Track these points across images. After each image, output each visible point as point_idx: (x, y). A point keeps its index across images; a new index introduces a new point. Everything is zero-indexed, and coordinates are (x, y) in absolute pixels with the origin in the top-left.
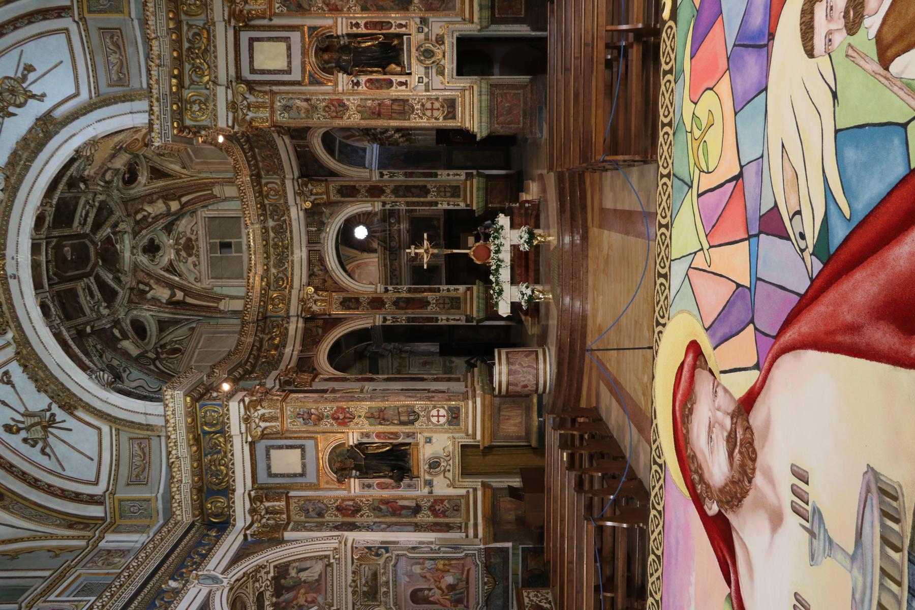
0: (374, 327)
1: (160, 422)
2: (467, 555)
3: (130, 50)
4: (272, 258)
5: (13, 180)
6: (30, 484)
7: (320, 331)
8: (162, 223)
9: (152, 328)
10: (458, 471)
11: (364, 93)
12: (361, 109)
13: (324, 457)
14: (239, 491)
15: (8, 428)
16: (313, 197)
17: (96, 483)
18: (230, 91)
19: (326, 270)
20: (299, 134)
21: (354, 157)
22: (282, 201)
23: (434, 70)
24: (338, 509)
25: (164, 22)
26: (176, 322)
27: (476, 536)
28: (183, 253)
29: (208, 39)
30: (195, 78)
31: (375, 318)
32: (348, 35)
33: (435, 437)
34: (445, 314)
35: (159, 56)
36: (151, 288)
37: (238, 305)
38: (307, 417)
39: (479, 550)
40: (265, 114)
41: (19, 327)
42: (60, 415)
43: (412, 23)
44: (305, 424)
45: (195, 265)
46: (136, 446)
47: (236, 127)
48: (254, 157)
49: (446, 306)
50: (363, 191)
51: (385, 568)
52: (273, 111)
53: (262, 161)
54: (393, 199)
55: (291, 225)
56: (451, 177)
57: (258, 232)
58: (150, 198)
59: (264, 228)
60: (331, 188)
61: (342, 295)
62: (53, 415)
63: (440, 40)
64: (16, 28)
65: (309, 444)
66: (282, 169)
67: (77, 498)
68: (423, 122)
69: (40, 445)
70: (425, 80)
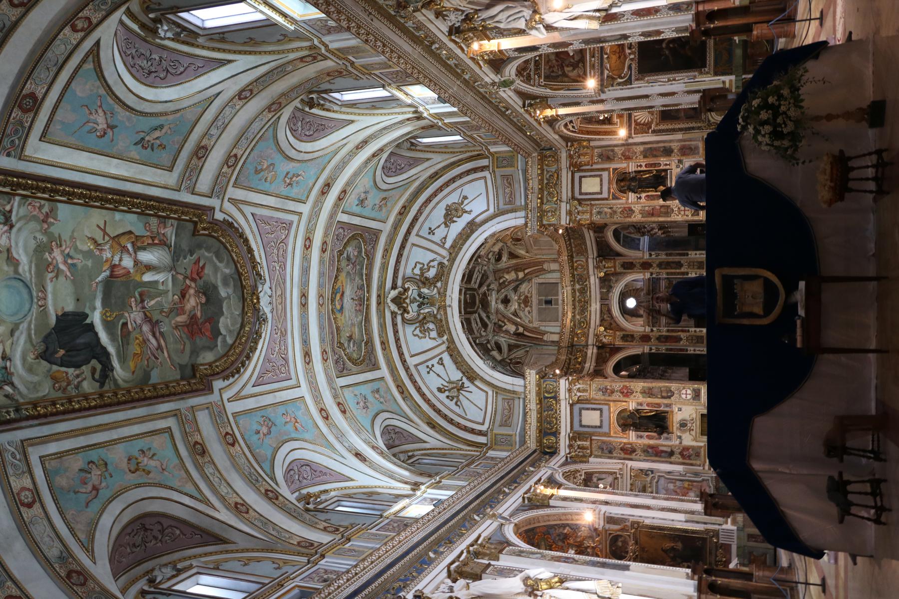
0: (643, 354)
1: (521, 389)
2: (703, 480)
3: (516, 186)
5: (453, 255)
6: (448, 422)
7: (608, 355)
8: (513, 285)
9: (505, 348)
10: (699, 431)
11: (644, 203)
12: (642, 212)
13: (614, 417)
15: (439, 390)
16: (605, 270)
17: (483, 424)
18: (568, 205)
19: (612, 317)
20: (599, 229)
21: (632, 244)
22: (585, 272)
24: (622, 449)
26: (517, 346)
28: (522, 305)
29: (558, 178)
30: (549, 199)
33: (684, 408)
34: (693, 346)
36: (505, 324)
37: (555, 338)
38: (605, 391)
40: (587, 216)
41: (450, 333)
42: (467, 383)
43: (673, 163)
44: (603, 395)
45: (529, 313)
48: (570, 244)
50: (638, 265)
51: (650, 483)
53: (575, 247)
54: (658, 270)
55: (590, 288)
56: (698, 256)
57: (570, 292)
58: (507, 270)
59: (573, 289)
62: (463, 383)
64: (461, 178)
65: (605, 408)
67: (472, 431)
68: (679, 218)
69: (455, 400)
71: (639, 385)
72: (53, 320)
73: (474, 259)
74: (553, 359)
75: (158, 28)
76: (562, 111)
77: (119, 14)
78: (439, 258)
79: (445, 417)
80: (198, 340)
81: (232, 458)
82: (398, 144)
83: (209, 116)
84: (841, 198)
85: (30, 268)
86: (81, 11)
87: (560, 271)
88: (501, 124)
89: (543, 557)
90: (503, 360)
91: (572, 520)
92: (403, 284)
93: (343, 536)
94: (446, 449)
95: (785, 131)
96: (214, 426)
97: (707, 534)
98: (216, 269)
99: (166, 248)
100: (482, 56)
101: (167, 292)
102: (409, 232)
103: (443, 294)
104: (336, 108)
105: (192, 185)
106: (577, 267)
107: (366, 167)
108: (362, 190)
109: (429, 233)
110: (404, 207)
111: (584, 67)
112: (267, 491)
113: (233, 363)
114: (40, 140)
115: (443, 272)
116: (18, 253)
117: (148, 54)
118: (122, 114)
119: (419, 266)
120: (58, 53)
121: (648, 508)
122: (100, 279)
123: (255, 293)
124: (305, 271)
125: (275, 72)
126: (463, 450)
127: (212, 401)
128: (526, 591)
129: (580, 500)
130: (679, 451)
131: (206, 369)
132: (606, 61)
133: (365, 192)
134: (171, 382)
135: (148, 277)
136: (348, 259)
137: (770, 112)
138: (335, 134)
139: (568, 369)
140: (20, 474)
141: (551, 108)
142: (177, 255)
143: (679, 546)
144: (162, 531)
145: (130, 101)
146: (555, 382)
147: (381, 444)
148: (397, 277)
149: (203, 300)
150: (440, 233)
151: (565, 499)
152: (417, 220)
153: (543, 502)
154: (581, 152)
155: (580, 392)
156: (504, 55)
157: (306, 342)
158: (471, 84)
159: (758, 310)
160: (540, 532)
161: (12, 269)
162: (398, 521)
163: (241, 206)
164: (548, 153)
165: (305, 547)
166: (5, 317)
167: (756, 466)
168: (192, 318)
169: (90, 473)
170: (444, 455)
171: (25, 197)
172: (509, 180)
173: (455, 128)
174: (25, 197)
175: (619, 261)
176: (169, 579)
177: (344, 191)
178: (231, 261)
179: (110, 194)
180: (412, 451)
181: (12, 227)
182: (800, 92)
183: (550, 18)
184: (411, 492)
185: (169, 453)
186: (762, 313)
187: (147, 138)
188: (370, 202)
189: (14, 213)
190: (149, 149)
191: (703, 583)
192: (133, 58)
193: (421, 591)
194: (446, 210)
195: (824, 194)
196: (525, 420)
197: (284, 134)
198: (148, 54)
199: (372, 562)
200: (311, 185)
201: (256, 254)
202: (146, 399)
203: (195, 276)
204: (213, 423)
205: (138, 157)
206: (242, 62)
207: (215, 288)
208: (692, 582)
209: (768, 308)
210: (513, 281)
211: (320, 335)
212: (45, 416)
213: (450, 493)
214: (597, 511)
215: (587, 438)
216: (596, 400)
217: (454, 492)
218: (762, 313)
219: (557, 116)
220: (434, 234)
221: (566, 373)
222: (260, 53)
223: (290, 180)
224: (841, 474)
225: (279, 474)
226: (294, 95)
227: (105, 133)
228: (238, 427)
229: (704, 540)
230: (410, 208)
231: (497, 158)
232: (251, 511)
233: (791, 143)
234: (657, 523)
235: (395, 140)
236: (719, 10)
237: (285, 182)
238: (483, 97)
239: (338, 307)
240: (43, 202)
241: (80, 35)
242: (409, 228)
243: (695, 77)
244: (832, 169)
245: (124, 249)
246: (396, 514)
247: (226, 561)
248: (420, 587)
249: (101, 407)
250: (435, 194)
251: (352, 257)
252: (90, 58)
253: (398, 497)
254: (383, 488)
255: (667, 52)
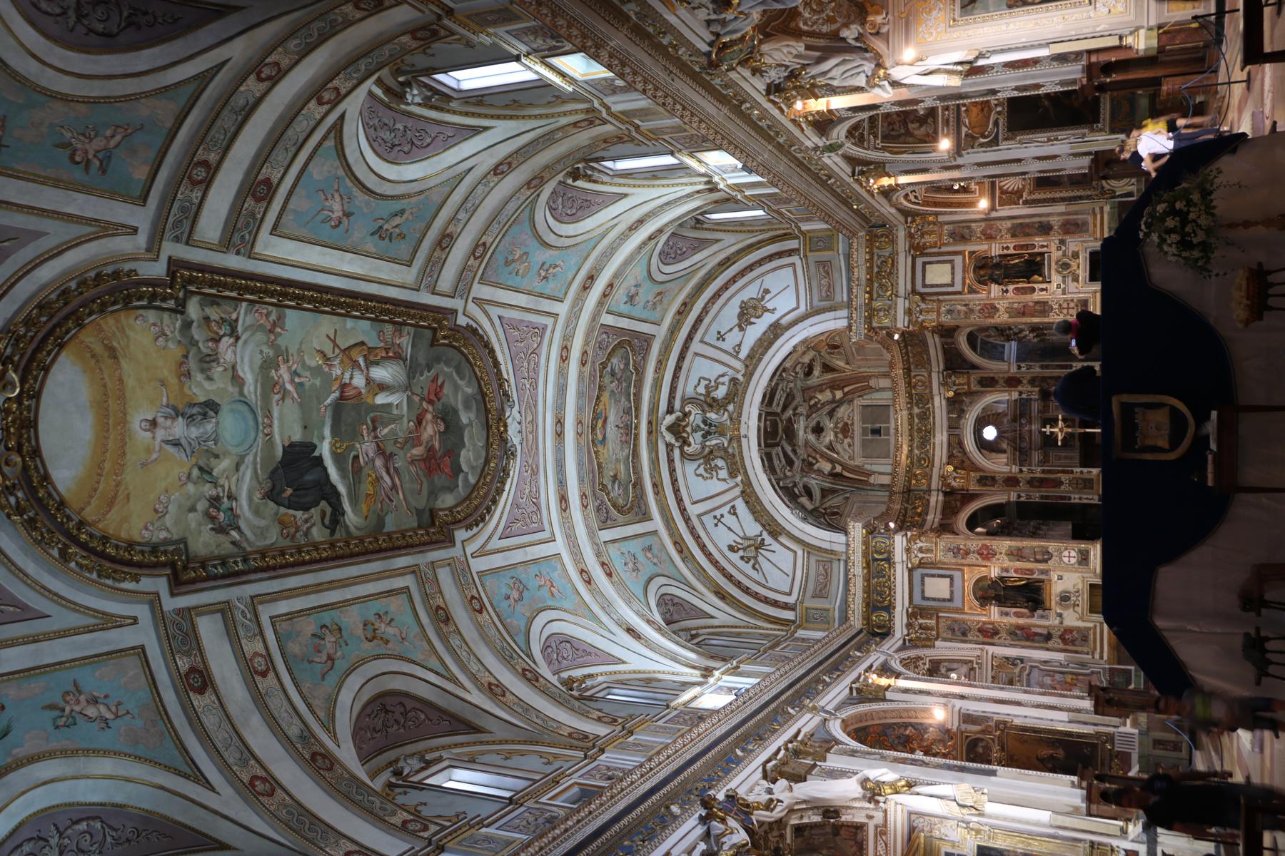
0: (1008, 503)
1: (842, 549)
2: (1093, 673)
3: (836, 275)
4: (916, 440)
5: (751, 368)
6: (743, 591)
7: (958, 504)
8: (827, 409)
9: (817, 494)
10: (1086, 606)
13: (969, 587)
14: (899, 608)
15: (731, 548)
16: (955, 388)
17: (790, 594)
18: (907, 301)
19: (964, 452)
20: (947, 333)
21: (992, 352)
22: (927, 391)
23: (1070, 278)
24: (980, 630)
25: (863, 255)
26: (833, 491)
27: (1101, 657)
28: (840, 436)
31: (1009, 495)
32: (1000, 256)
34: (1079, 493)
35: (858, 279)
36: (817, 461)
37: (886, 480)
38: (956, 551)
39: (1104, 669)
40: (933, 316)
41: (746, 473)
42: (768, 539)
43: (1052, 244)
45: (850, 445)
46: (821, 568)
47: (911, 327)
48: (907, 353)
49: (1080, 486)
50: (1001, 382)
52: (939, 314)
54: (1030, 388)
55: (934, 412)
57: (905, 418)
58: (820, 388)
59: (910, 414)
60: (972, 379)
61: (978, 475)
62: (763, 540)
63: (1076, 255)
65: (957, 574)
66: (930, 364)
67: (775, 604)
69: (752, 562)
70: (1062, 286)
71: (1003, 545)
72: (279, 452)
73: (778, 373)
74: (883, 508)
75: (406, 92)
76: (903, 180)
77: (370, 84)
78: (731, 372)
79: (738, 585)
80: (436, 477)
81: (480, 628)
82: (681, 223)
83: (457, 197)
84: (1260, 317)
85: (256, 387)
86: (269, 54)
87: (893, 389)
88: (821, 196)
89: (883, 758)
90: (815, 509)
91: (916, 718)
92: (683, 407)
93: (623, 728)
94: (740, 627)
95: (1195, 241)
96: (457, 588)
97: (1098, 739)
98: (456, 388)
99: (401, 363)
100: (806, 117)
101: (401, 417)
102: (690, 338)
103: (736, 420)
104: (606, 179)
105: (433, 283)
106: (916, 384)
107: (639, 252)
108: (633, 282)
109: (718, 339)
110: (685, 304)
111: (935, 122)
112: (524, 670)
113: (477, 508)
114: (271, 234)
115: (737, 391)
116: (243, 371)
117: (391, 124)
118: (360, 197)
119: (703, 383)
120: (298, 130)
121: (1018, 704)
122: (328, 401)
123: (501, 420)
124: (561, 390)
125: (541, 140)
126: (763, 629)
127: (454, 555)
128: (864, 797)
129: (928, 693)
130: (1059, 633)
131: (446, 515)
132: (963, 114)
133: (636, 286)
134: (407, 531)
135: (381, 399)
136: (613, 374)
137: (1177, 219)
138: (603, 211)
139: (903, 522)
140: (251, 637)
141: (890, 176)
142: (412, 371)
143: (1060, 753)
144: (405, 714)
145: (371, 181)
146: (889, 539)
147: (658, 618)
148: (674, 398)
149: (442, 428)
150: (732, 339)
151: (906, 691)
152: (701, 321)
153: (878, 695)
154: (925, 229)
155: (922, 552)
156: (834, 115)
157: (561, 483)
158: (785, 149)
159: (1163, 443)
160: (875, 733)
161: (237, 389)
162: (690, 713)
163: (486, 307)
164: (880, 231)
165: (579, 739)
166: (230, 448)
167: (1160, 623)
168: (429, 451)
169: (324, 639)
170: (739, 635)
171: (252, 302)
172: (826, 268)
173: (758, 202)
174: (252, 302)
175: (975, 376)
176: (418, 772)
177: (611, 285)
178: (474, 379)
179: (342, 296)
180: (695, 629)
181: (237, 338)
182: (1213, 197)
183: (897, 73)
184: (701, 679)
185: (409, 618)
186: (1167, 446)
187: (385, 227)
188: (641, 299)
189: (240, 322)
190: (387, 239)
191: (1094, 791)
192: (375, 130)
193: (734, 791)
194: (741, 307)
195: (1240, 313)
196: (847, 590)
197: (542, 214)
198: (391, 124)
199: (668, 757)
200: (570, 277)
201: (503, 368)
202: (380, 551)
203: (433, 397)
204: (455, 583)
205: (374, 250)
206: (501, 129)
207: (456, 412)
208: (1079, 791)
209: (1175, 441)
210: (828, 403)
211: (579, 473)
212: (274, 568)
213: (754, 681)
214: (950, 706)
215: (932, 615)
216: (944, 563)
217: (758, 680)
218: (1167, 446)
219: (897, 185)
220: (724, 340)
221: (900, 528)
222: (524, 117)
223: (546, 272)
224: (1258, 630)
225: (536, 650)
226: (559, 167)
227: (340, 222)
228: (484, 590)
229: (1094, 746)
230: (692, 306)
231: (810, 238)
232: (508, 694)
233: (1202, 254)
234: (1030, 723)
235: (679, 218)
236: (1117, 62)
237: (540, 275)
238: (800, 164)
239: (600, 437)
240: (270, 308)
241: (326, 107)
242: (690, 332)
243: (1084, 136)
244: (1248, 284)
245: (355, 364)
246: (686, 704)
247: (483, 753)
248: (732, 785)
249: (333, 559)
250: (725, 287)
251: (617, 371)
252: (332, 135)
253: (685, 686)
254: (664, 673)
255: (1046, 103)
